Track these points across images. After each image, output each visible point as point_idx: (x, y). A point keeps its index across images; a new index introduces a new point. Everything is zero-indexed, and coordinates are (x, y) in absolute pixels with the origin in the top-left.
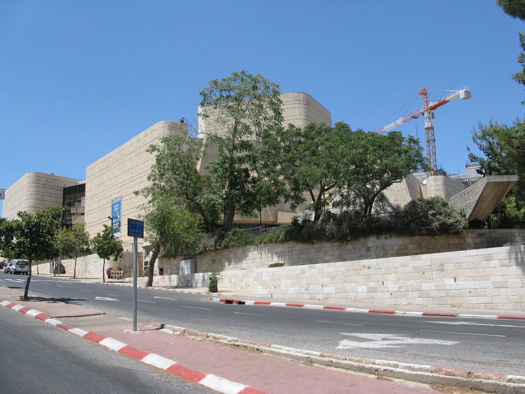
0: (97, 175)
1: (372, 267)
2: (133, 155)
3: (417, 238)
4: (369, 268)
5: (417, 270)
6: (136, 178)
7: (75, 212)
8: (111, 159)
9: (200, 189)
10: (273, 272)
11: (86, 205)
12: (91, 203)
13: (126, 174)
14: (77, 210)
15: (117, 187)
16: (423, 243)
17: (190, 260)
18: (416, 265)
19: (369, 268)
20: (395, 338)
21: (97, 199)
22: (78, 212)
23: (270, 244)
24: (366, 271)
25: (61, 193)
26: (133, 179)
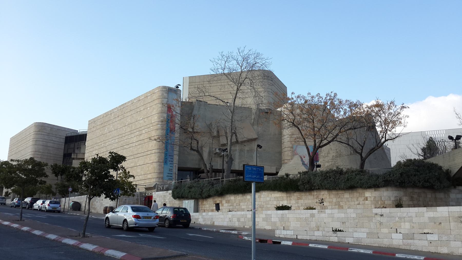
0: (98, 127)
1: (384, 215)
2: (132, 112)
3: (410, 190)
4: (382, 215)
5: (432, 220)
6: (135, 131)
7: (75, 157)
8: (113, 115)
9: (221, 145)
10: (282, 214)
11: (86, 152)
12: (91, 150)
13: (126, 127)
14: (77, 156)
15: (117, 137)
16: (414, 196)
17: (193, 201)
18: (432, 216)
19: (382, 215)
20: (229, 231)
21: (97, 147)
22: (78, 157)
23: (62, 153)
24: (379, 218)
25: (63, 141)
26: (133, 132)
